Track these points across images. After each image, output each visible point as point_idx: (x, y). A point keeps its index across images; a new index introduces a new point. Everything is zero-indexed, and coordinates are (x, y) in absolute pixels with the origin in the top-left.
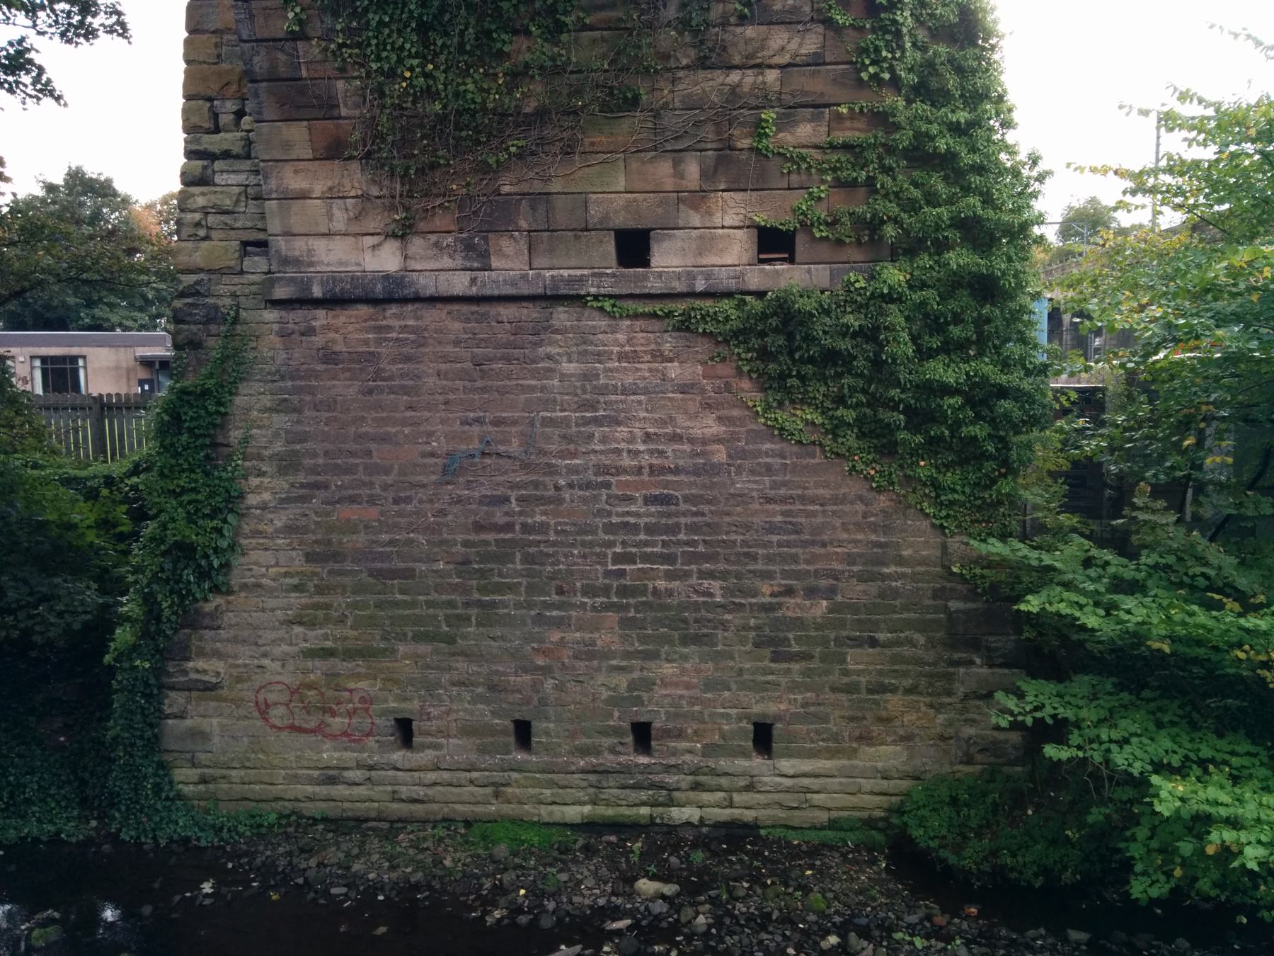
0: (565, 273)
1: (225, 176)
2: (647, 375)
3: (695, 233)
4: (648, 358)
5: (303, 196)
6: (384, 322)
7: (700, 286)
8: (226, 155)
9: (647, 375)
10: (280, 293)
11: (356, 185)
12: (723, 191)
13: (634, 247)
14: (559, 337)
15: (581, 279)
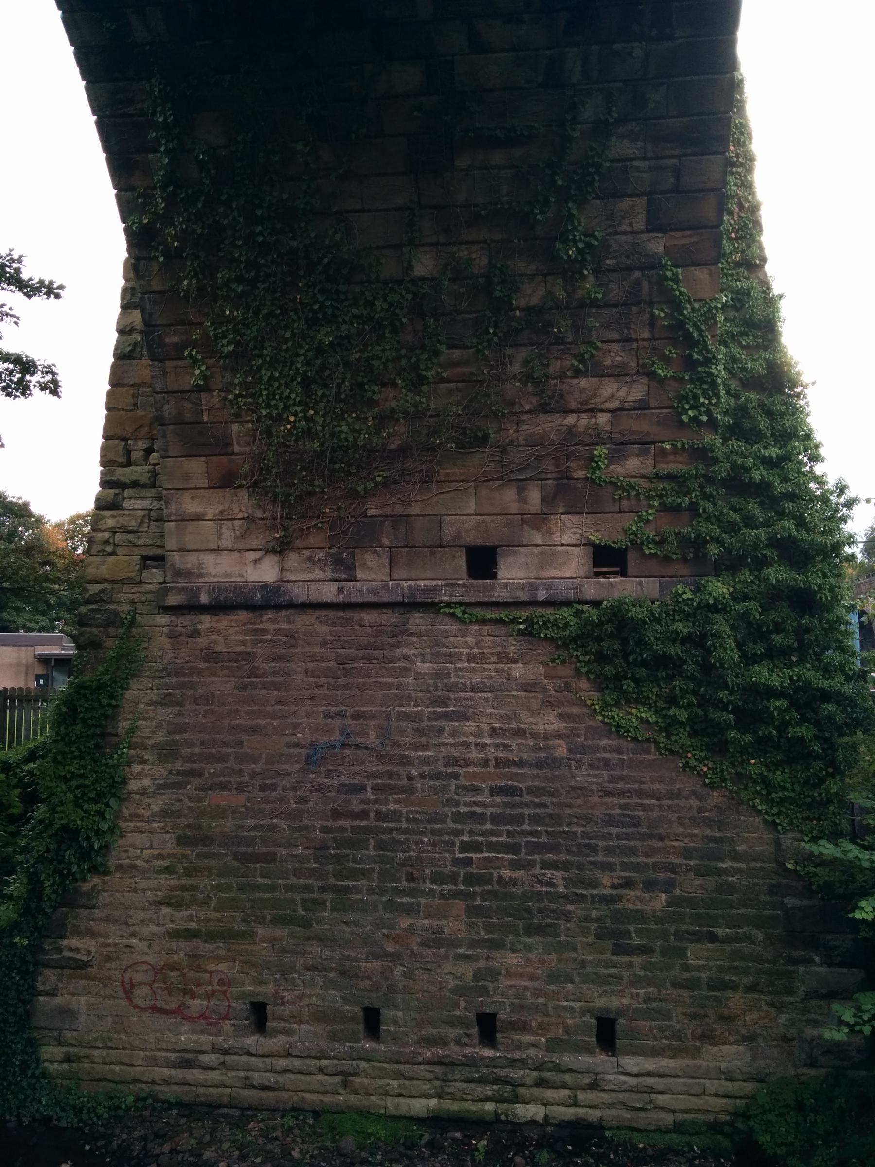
0: (422, 583)
1: (133, 502)
2: (494, 674)
3: (536, 550)
4: (494, 659)
5: (198, 518)
6: (261, 626)
7: (542, 595)
8: (135, 484)
9: (494, 674)
10: (172, 600)
11: (243, 509)
12: (562, 514)
13: (482, 561)
14: (415, 639)
15: (436, 589)
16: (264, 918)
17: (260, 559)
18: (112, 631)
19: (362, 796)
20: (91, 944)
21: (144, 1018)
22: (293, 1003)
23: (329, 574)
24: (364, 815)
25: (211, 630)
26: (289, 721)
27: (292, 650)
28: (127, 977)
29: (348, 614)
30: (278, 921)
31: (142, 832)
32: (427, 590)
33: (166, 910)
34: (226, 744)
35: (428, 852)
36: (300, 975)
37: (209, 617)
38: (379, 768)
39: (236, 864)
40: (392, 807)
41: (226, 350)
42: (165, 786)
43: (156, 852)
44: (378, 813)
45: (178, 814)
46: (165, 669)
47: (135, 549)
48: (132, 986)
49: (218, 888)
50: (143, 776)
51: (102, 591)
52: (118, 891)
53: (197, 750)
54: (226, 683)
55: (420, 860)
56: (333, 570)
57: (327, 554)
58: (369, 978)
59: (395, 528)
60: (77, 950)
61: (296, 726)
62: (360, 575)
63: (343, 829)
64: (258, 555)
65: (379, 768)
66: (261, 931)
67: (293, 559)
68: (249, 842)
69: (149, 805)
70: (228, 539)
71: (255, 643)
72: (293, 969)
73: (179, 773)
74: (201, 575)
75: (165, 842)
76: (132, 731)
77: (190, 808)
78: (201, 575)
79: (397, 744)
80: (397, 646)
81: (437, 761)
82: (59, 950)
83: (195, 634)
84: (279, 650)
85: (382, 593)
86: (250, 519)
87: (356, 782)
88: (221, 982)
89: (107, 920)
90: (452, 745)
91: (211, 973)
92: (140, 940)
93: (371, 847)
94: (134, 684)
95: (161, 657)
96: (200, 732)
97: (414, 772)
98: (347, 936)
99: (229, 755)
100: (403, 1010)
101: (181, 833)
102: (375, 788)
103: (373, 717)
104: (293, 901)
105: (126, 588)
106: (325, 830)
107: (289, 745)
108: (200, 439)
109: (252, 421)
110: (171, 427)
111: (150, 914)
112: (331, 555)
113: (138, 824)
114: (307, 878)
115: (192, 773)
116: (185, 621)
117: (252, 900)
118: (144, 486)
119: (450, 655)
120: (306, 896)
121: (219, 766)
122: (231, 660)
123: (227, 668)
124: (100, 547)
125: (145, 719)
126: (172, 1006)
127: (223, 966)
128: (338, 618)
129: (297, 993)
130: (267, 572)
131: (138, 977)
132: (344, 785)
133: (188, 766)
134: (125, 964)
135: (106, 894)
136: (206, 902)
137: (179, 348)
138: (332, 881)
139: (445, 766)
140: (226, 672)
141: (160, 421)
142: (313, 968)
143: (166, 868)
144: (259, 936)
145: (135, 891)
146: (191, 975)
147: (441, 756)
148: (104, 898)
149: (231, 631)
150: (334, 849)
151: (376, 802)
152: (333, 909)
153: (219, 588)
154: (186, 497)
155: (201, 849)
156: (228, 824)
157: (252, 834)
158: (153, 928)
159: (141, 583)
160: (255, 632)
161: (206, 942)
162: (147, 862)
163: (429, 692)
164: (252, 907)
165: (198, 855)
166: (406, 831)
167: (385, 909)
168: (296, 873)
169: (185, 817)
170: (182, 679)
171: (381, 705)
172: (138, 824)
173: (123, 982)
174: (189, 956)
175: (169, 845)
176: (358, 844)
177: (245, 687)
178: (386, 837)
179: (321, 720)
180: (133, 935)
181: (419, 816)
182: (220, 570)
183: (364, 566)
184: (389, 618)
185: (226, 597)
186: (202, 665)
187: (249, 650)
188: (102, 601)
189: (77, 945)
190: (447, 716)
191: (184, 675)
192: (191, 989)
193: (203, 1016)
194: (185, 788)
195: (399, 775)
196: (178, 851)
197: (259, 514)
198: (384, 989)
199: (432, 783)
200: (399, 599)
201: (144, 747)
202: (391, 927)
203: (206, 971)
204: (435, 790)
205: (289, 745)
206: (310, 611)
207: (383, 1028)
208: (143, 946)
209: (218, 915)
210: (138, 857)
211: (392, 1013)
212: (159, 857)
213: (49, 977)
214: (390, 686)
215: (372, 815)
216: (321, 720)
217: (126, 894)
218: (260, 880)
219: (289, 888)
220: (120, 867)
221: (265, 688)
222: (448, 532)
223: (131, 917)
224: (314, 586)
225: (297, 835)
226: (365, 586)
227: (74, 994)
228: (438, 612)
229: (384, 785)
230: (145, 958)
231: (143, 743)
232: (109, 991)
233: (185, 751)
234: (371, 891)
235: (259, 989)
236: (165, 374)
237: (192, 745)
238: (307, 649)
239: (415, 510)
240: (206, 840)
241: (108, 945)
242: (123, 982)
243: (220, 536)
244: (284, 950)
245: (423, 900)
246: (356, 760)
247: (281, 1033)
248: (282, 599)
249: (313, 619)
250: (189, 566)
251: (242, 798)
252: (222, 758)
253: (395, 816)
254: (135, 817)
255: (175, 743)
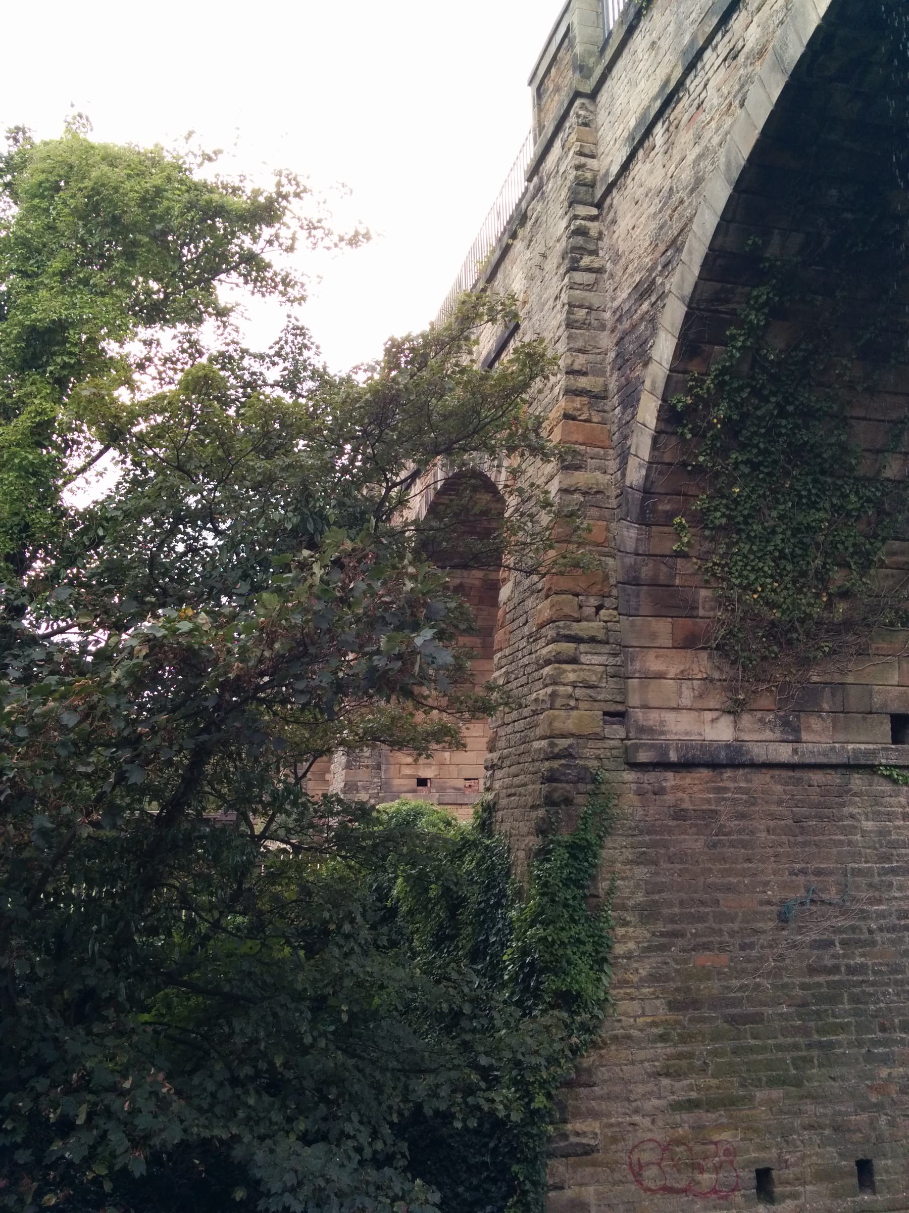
0: (863, 747)
1: (589, 657)
5: (661, 676)
8: (592, 640)
10: (643, 757)
14: (857, 799)
15: (874, 753)
16: (760, 1080)
17: (717, 719)
18: (581, 787)
19: (831, 952)
20: (596, 1126)
21: (656, 1201)
22: (795, 1164)
23: (778, 735)
24: (835, 969)
25: (677, 788)
26: (758, 879)
27: (752, 808)
28: (635, 1158)
29: (798, 774)
30: (774, 1082)
31: (633, 999)
32: (867, 753)
33: (665, 1082)
34: (703, 903)
35: (895, 1002)
36: (799, 1135)
37: (672, 774)
38: (843, 923)
39: (726, 1026)
40: (859, 960)
41: (717, 522)
42: (649, 949)
43: (649, 1020)
44: (848, 967)
45: (667, 978)
46: (637, 826)
47: (595, 704)
48: (641, 1167)
49: (714, 1053)
50: (628, 939)
51: (570, 746)
52: (616, 1065)
53: (676, 910)
54: (696, 841)
55: (890, 1010)
56: (781, 732)
57: (776, 716)
58: (860, 1131)
59: (833, 695)
60: (584, 1134)
61: (766, 884)
62: (805, 736)
63: (819, 985)
64: (715, 714)
65: (843, 923)
66: (759, 1095)
67: (746, 719)
68: (734, 1003)
69: (637, 970)
70: (687, 699)
71: (719, 801)
72: (793, 1130)
73: (662, 935)
74: (663, 733)
75: (657, 1008)
76: (610, 892)
77: (677, 971)
78: (663, 733)
79: (854, 899)
80: (843, 805)
81: (891, 914)
82: (565, 1136)
83: (660, 792)
84: (741, 808)
85: (831, 755)
86: (708, 680)
87: (825, 937)
88: (727, 1152)
89: (608, 1097)
90: (901, 899)
91: (716, 1143)
92: (643, 1116)
93: (846, 1001)
94: (608, 842)
95: (632, 814)
96: (678, 891)
97: (874, 926)
98: (837, 1091)
99: (708, 913)
100: (891, 1158)
101: (671, 998)
102: (843, 943)
103: (831, 873)
104: (784, 1060)
105: (591, 744)
106: (804, 986)
107: (762, 903)
108: (670, 601)
109: (723, 588)
110: (645, 588)
111: (650, 1087)
112: (780, 718)
113: (628, 991)
114: (793, 1036)
115: (675, 934)
116: (650, 777)
117: (746, 1063)
118: (600, 642)
119: (889, 814)
120: (795, 1054)
121: (700, 926)
122: (697, 817)
123: (696, 826)
124: (564, 701)
125: (623, 879)
126: (683, 1184)
127: (725, 1136)
128: (790, 778)
129: (799, 1154)
130: (721, 731)
131: (646, 1157)
132: (815, 941)
133: (670, 927)
134: (630, 1144)
135: (604, 1069)
136: (703, 1070)
137: (671, 515)
138: (816, 1037)
139: (898, 919)
140: (694, 830)
141: (636, 582)
142: (811, 1127)
143: (661, 1036)
144: (758, 1100)
145: (633, 1063)
146: (698, 1148)
147: (894, 909)
148: (602, 1073)
149: (695, 789)
150: (814, 1004)
151: (844, 956)
152: (821, 1065)
153: (684, 745)
154: (651, 655)
155: (691, 1013)
156: (715, 986)
157: (739, 994)
158: (655, 1102)
159: (605, 738)
160: (718, 790)
161: (708, 1111)
162: (641, 1030)
163: (875, 849)
164: (748, 1070)
165: (690, 1020)
166: (873, 984)
167: (865, 1061)
168: (784, 1032)
169: (673, 980)
170: (654, 837)
171: (837, 862)
172: (628, 991)
173: (631, 1164)
174: (693, 1128)
175: (661, 1011)
176: (833, 1000)
177: (714, 845)
178: (857, 990)
179: (786, 877)
180: (636, 1111)
181: (883, 968)
182: (680, 728)
183: (809, 728)
184: (834, 778)
185: (693, 756)
186: (672, 823)
187: (713, 808)
188: (570, 756)
189: (585, 1129)
190: (893, 871)
191: (656, 833)
192: (699, 1164)
193: (714, 1191)
194: (669, 950)
195: (861, 930)
196: (671, 1017)
197: (716, 675)
198: (873, 1140)
199: (889, 935)
200: (845, 761)
201: (624, 908)
202: (872, 1078)
203: (712, 1142)
204: (893, 942)
205: (762, 903)
206: (764, 771)
207: (877, 1178)
208: (647, 1122)
209: (716, 1081)
210: (631, 1026)
211: (883, 1162)
212: (654, 1024)
213: (558, 1168)
214: (841, 843)
215: (843, 969)
216: (786, 877)
217: (624, 1067)
218: (753, 1042)
219: (779, 1048)
220: (615, 1038)
221: (733, 846)
222: (877, 700)
223: (631, 1091)
224: (772, 746)
225: (779, 993)
226: (816, 748)
227: (581, 1185)
228: (875, 773)
229: (850, 939)
230: (649, 1135)
231: (623, 904)
232: (617, 1176)
233: (666, 911)
234: (850, 1044)
235: (763, 1155)
236: (650, 537)
237: (671, 905)
238: (766, 808)
239: (850, 679)
240: (695, 1004)
241: (612, 1125)
242: (631, 1164)
243: (680, 695)
244: (781, 1112)
245: (895, 1049)
246: (823, 916)
247: (788, 1197)
248: (744, 759)
249: (768, 779)
250: (651, 723)
251: (724, 958)
252: (701, 918)
253: (860, 969)
254: (625, 983)
255: (656, 902)
